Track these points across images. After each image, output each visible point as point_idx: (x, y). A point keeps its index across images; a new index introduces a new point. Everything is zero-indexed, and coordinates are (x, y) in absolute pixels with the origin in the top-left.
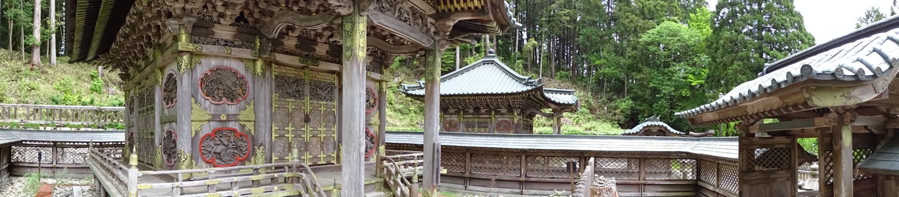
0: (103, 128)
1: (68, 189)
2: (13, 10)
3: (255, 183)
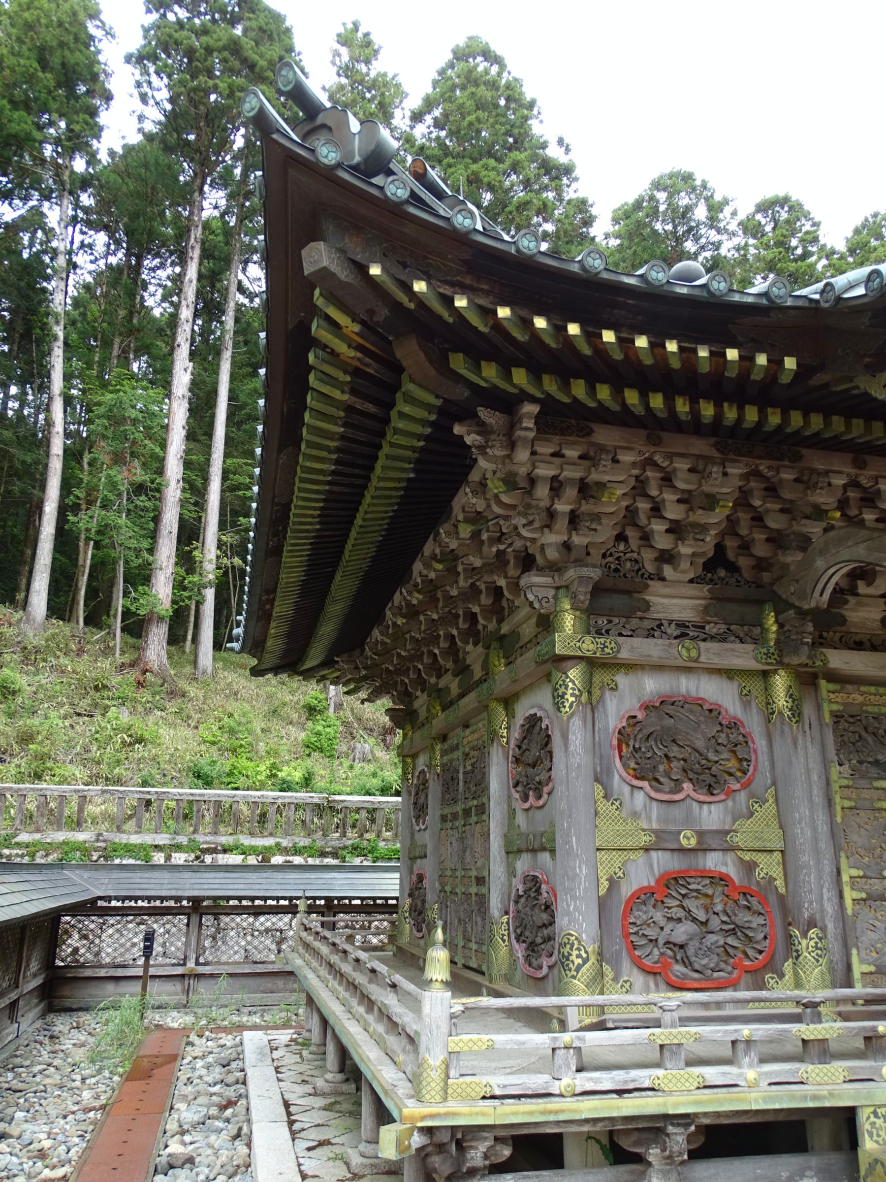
0: (335, 855)
1: (228, 1040)
2: (97, 511)
3: (814, 1050)
